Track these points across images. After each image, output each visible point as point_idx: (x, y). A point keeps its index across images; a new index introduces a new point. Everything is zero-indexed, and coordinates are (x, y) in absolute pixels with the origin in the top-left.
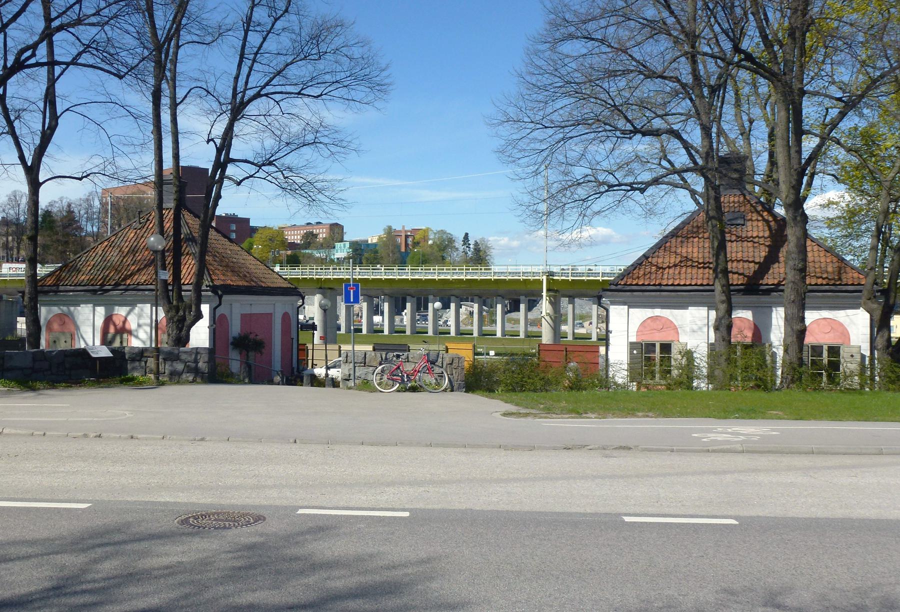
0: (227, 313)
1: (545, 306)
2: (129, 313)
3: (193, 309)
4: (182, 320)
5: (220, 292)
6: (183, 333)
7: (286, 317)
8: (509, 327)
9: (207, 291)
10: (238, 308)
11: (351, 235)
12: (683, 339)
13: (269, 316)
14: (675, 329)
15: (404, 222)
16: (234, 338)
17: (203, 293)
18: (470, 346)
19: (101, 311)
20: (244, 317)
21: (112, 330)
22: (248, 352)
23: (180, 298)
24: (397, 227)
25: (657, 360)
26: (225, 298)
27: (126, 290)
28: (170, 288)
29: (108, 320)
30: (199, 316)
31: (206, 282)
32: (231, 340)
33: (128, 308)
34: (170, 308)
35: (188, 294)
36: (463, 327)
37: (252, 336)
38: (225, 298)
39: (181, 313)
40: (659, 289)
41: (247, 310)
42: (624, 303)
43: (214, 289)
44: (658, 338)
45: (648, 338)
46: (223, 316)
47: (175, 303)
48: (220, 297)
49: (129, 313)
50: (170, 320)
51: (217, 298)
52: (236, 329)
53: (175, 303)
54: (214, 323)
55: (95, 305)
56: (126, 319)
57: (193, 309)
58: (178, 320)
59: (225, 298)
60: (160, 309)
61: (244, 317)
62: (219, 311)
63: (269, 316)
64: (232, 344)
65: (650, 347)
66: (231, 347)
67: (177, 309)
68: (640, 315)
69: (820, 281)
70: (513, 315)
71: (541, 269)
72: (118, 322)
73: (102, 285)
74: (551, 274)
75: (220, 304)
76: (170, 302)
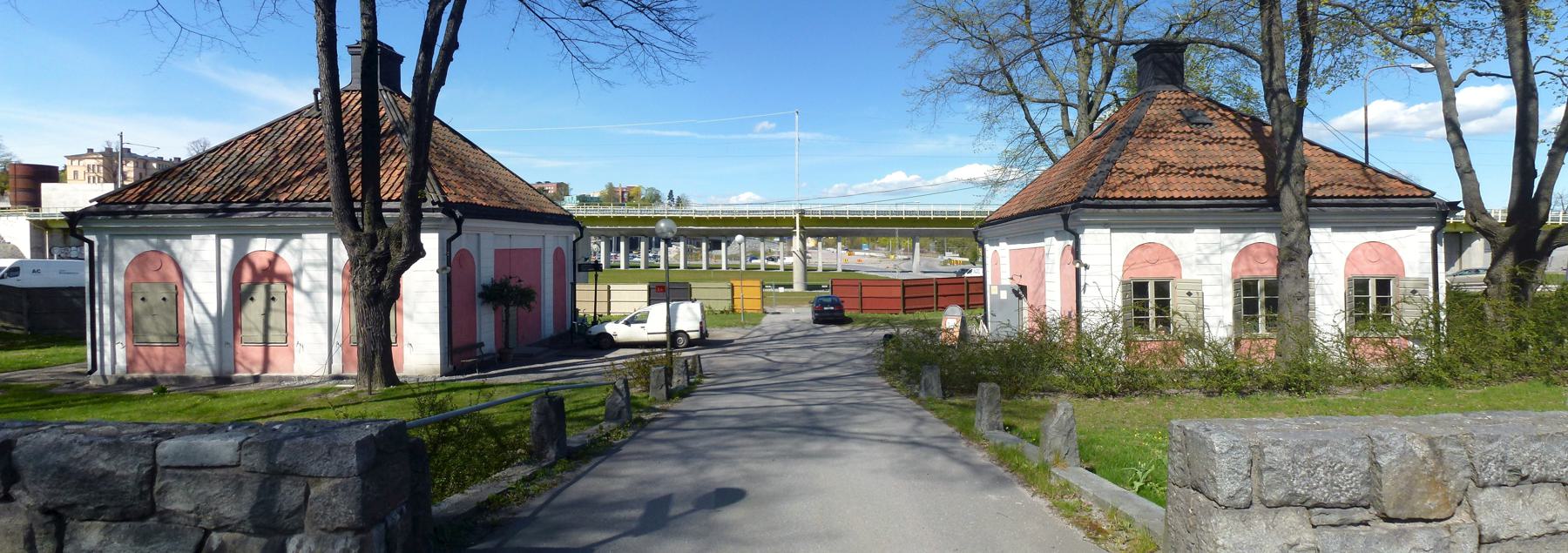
0: (472, 249)
1: (796, 240)
2: (282, 246)
3: (405, 240)
4: (381, 262)
5: (458, 214)
6: (385, 283)
7: (558, 253)
8: (712, 262)
9: (433, 210)
10: (489, 243)
11: (576, 191)
12: (1187, 274)
13: (537, 253)
14: (1175, 260)
15: (621, 183)
16: (484, 287)
17: (425, 215)
18: (758, 283)
19: (227, 244)
20: (499, 253)
21: (247, 276)
22: (508, 307)
23: (378, 220)
24: (616, 185)
25: (1152, 304)
26: (467, 223)
27: (274, 210)
28: (357, 205)
29: (242, 260)
30: (417, 252)
31: (432, 195)
32: (479, 290)
33: (279, 241)
34: (358, 239)
35: (393, 213)
36: (671, 262)
37: (513, 283)
38: (467, 223)
39: (380, 246)
40: (1152, 203)
41: (505, 244)
42: (1105, 225)
43: (447, 208)
44: (1151, 274)
45: (1139, 275)
46: (464, 253)
47: (367, 229)
48: (459, 222)
49: (282, 246)
50: (354, 262)
51: (453, 223)
52: (486, 271)
53: (367, 229)
54: (449, 264)
55: (219, 237)
56: (276, 255)
57: (405, 240)
58: (373, 261)
59: (468, 223)
60: (338, 243)
61: (499, 253)
62: (457, 245)
63: (537, 253)
64: (481, 295)
65: (1140, 288)
66: (479, 301)
67: (373, 241)
68: (1128, 241)
69: (1362, 192)
70: (715, 252)
71: (793, 208)
72: (261, 262)
73: (227, 201)
74: (802, 212)
75: (459, 233)
76: (355, 226)
